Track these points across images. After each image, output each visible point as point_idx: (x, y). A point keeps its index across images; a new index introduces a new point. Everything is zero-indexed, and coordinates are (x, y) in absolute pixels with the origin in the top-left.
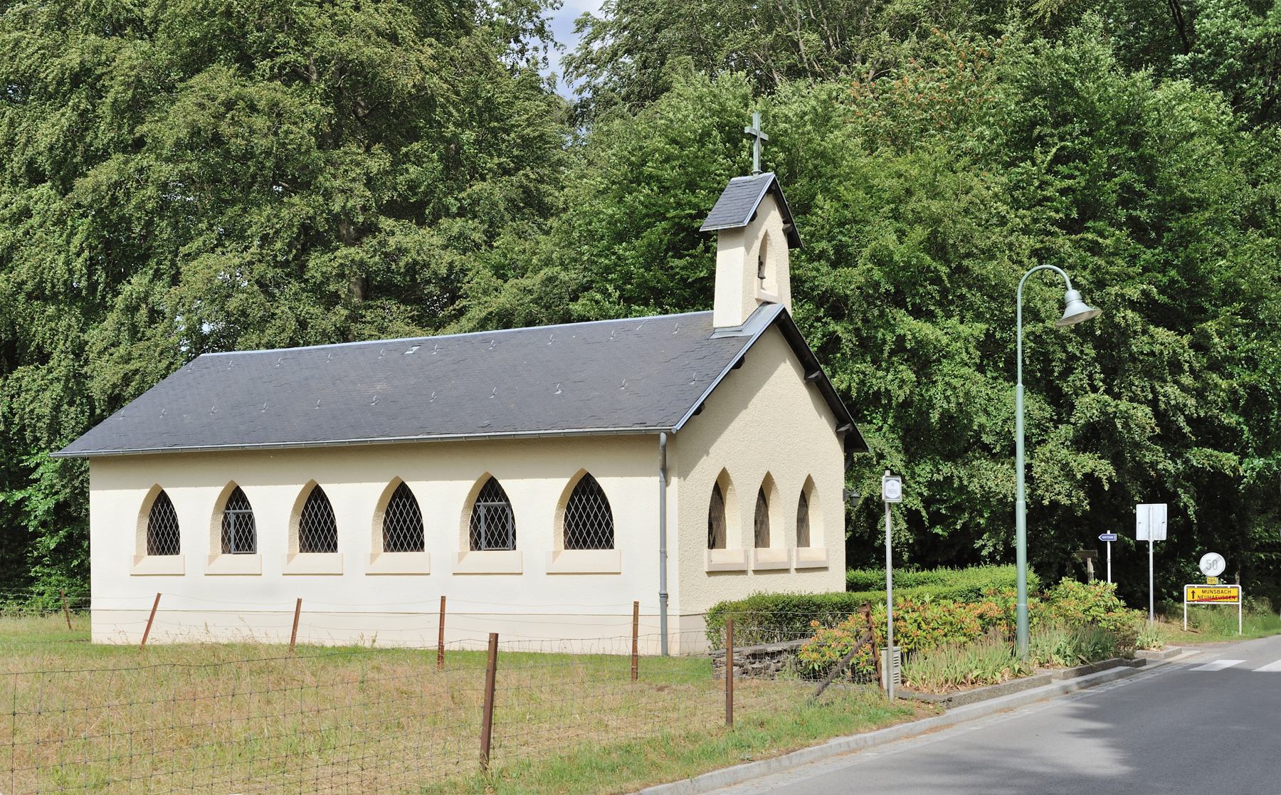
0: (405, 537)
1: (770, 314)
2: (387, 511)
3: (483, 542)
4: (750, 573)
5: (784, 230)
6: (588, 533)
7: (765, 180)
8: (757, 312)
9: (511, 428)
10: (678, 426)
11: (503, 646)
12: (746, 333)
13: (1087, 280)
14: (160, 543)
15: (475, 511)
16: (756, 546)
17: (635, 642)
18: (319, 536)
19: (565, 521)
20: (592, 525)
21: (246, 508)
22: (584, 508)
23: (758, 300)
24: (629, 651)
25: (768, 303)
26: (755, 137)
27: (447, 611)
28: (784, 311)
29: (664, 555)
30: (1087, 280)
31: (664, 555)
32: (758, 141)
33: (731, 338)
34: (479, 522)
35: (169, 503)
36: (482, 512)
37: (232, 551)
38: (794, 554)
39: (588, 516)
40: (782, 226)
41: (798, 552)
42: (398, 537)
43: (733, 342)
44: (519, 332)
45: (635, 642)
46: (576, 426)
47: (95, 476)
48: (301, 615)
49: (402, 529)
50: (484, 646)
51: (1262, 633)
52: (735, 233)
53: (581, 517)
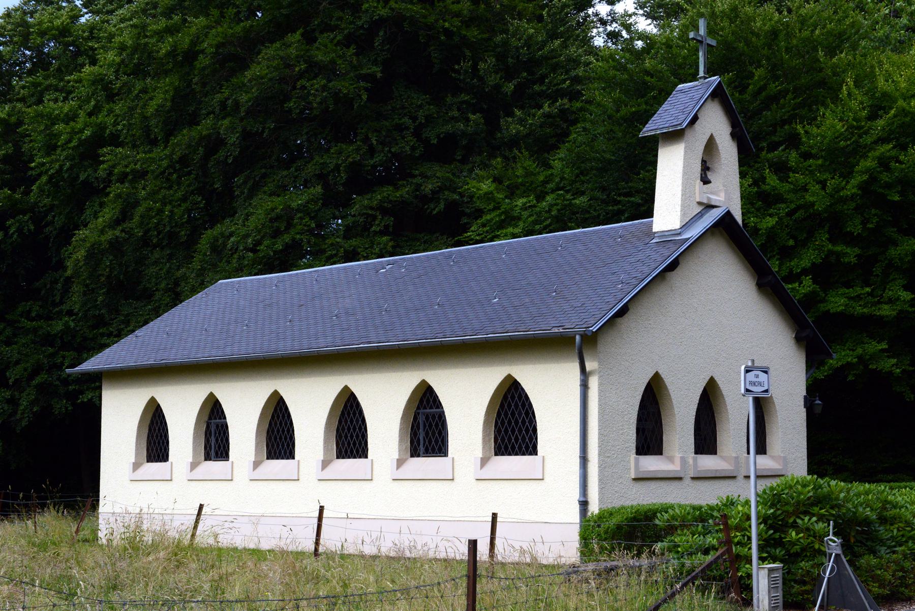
0: (354, 444)
1: (712, 216)
3: (213, 453)
4: (740, 478)
6: (517, 439)
7: (710, 84)
8: (700, 215)
9: (440, 335)
14: (157, 451)
15: (415, 418)
16: (696, 453)
18: (283, 444)
19: (495, 427)
20: (520, 431)
21: (220, 418)
22: (513, 414)
23: (700, 203)
28: (728, 214)
29: (584, 460)
31: (584, 460)
33: (668, 239)
34: (419, 429)
35: (437, 404)
36: (421, 419)
37: (212, 459)
38: (691, 461)
39: (517, 422)
41: (695, 460)
42: (349, 444)
43: (670, 245)
48: (324, 521)
49: (352, 437)
50: (464, 549)
51: (99, 539)
52: (675, 136)
53: (510, 422)
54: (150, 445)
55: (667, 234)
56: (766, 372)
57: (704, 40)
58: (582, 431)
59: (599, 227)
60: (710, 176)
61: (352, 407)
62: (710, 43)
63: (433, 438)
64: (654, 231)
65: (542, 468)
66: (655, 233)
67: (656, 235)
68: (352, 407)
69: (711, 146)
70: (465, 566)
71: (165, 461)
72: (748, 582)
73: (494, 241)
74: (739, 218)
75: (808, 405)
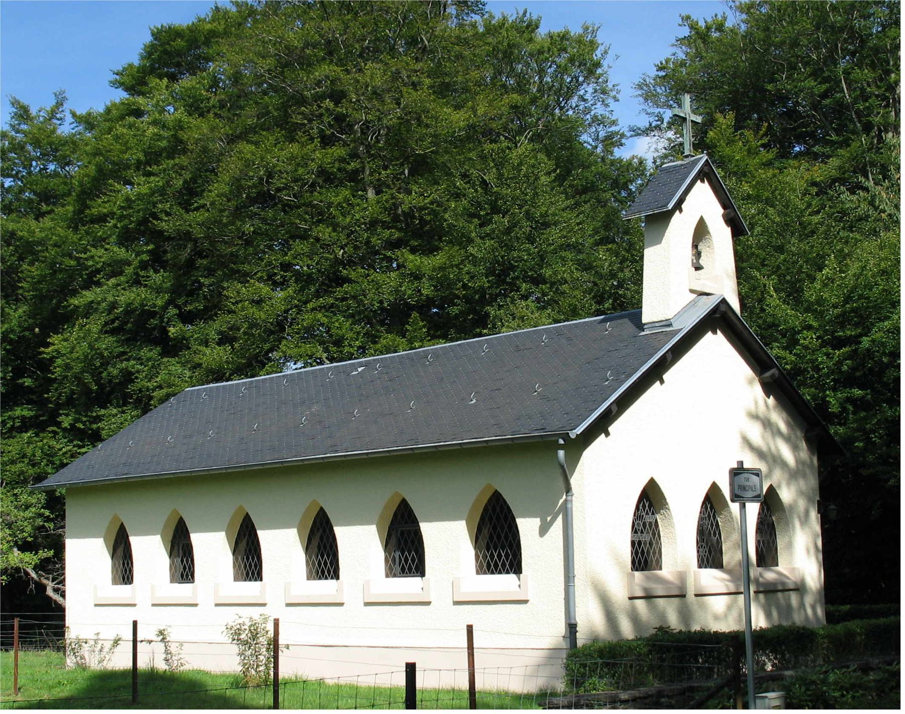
2: (488, 543)
5: (724, 216)
8: (692, 304)
10: (579, 430)
11: (421, 682)
12: (676, 327)
13: (591, 145)
17: (16, 679)
24: (465, 686)
25: (708, 294)
26: (684, 119)
27: (476, 644)
28: (724, 301)
30: (591, 145)
32: (689, 124)
40: (720, 211)
44: (459, 345)
45: (16, 679)
46: (475, 436)
47: (73, 513)
50: (400, 680)
54: (322, 541)
55: (657, 325)
56: (757, 475)
57: (687, 117)
58: (570, 539)
59: (475, 340)
60: (702, 262)
61: (247, 527)
62: (695, 120)
63: (510, 541)
64: (643, 322)
65: (168, 608)
66: (645, 324)
67: (645, 327)
68: (247, 527)
69: (701, 232)
70: (467, 695)
71: (130, 584)
72: (739, 704)
73: (232, 380)
74: (735, 305)
75: (822, 511)
